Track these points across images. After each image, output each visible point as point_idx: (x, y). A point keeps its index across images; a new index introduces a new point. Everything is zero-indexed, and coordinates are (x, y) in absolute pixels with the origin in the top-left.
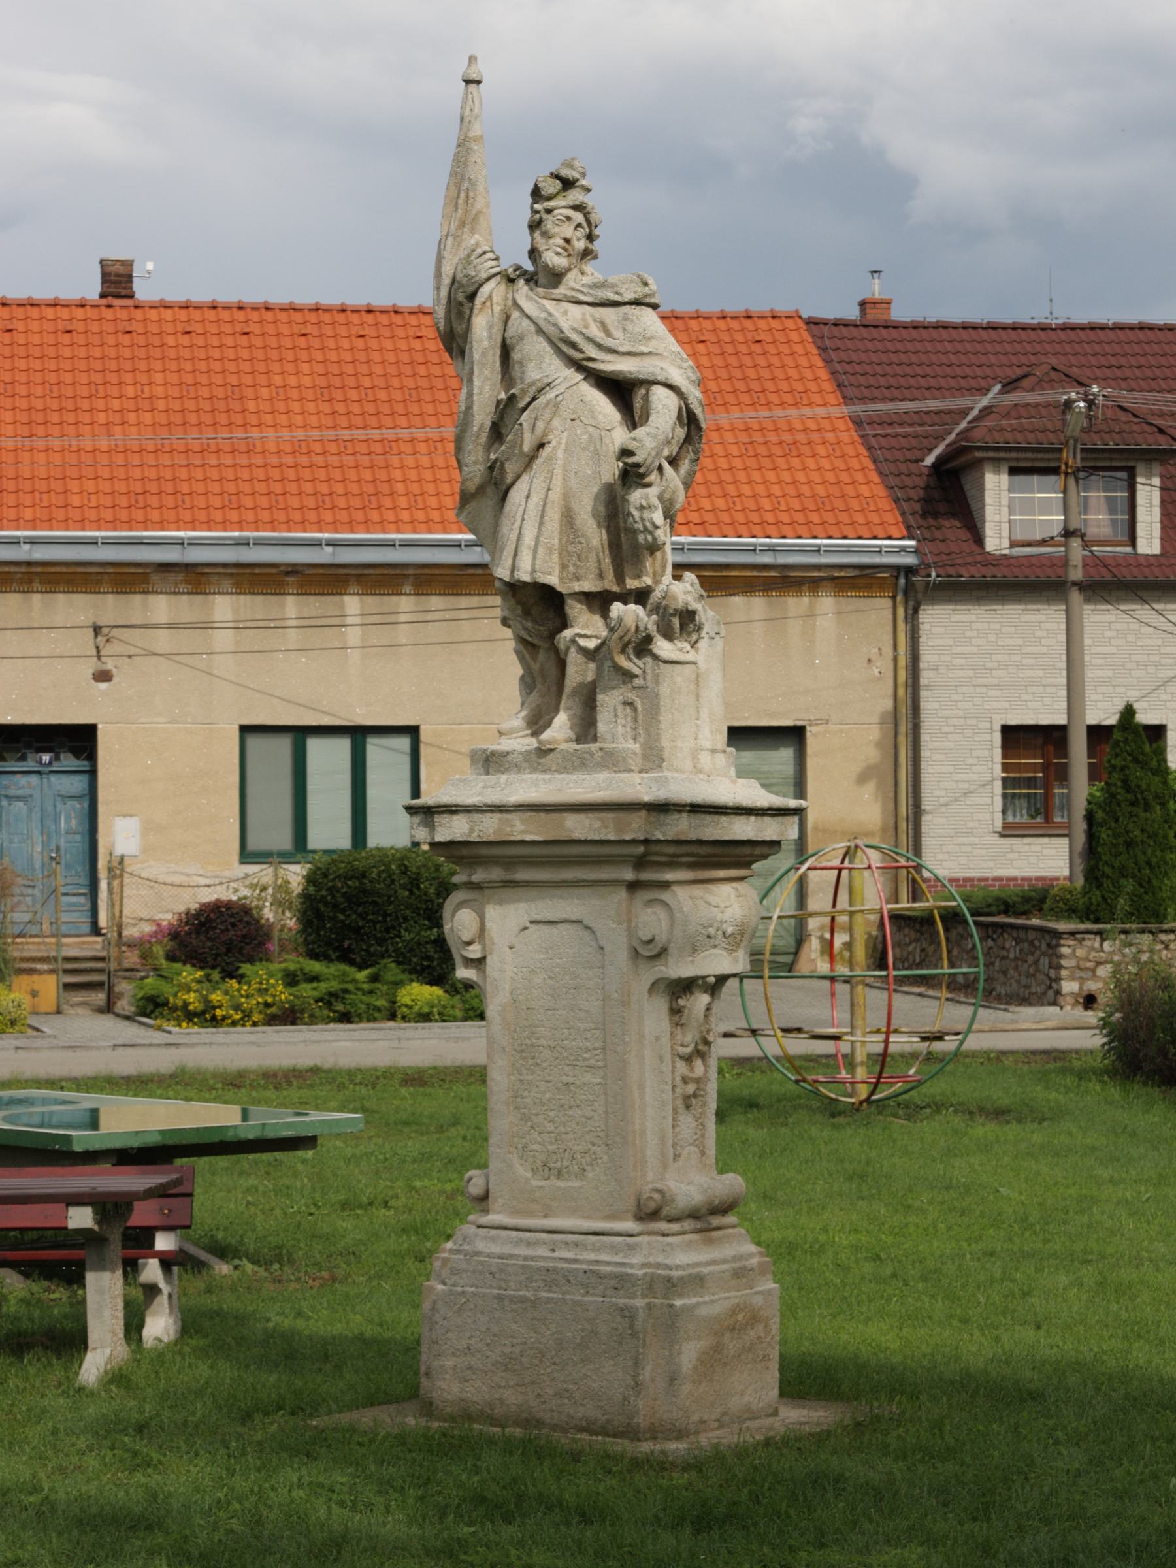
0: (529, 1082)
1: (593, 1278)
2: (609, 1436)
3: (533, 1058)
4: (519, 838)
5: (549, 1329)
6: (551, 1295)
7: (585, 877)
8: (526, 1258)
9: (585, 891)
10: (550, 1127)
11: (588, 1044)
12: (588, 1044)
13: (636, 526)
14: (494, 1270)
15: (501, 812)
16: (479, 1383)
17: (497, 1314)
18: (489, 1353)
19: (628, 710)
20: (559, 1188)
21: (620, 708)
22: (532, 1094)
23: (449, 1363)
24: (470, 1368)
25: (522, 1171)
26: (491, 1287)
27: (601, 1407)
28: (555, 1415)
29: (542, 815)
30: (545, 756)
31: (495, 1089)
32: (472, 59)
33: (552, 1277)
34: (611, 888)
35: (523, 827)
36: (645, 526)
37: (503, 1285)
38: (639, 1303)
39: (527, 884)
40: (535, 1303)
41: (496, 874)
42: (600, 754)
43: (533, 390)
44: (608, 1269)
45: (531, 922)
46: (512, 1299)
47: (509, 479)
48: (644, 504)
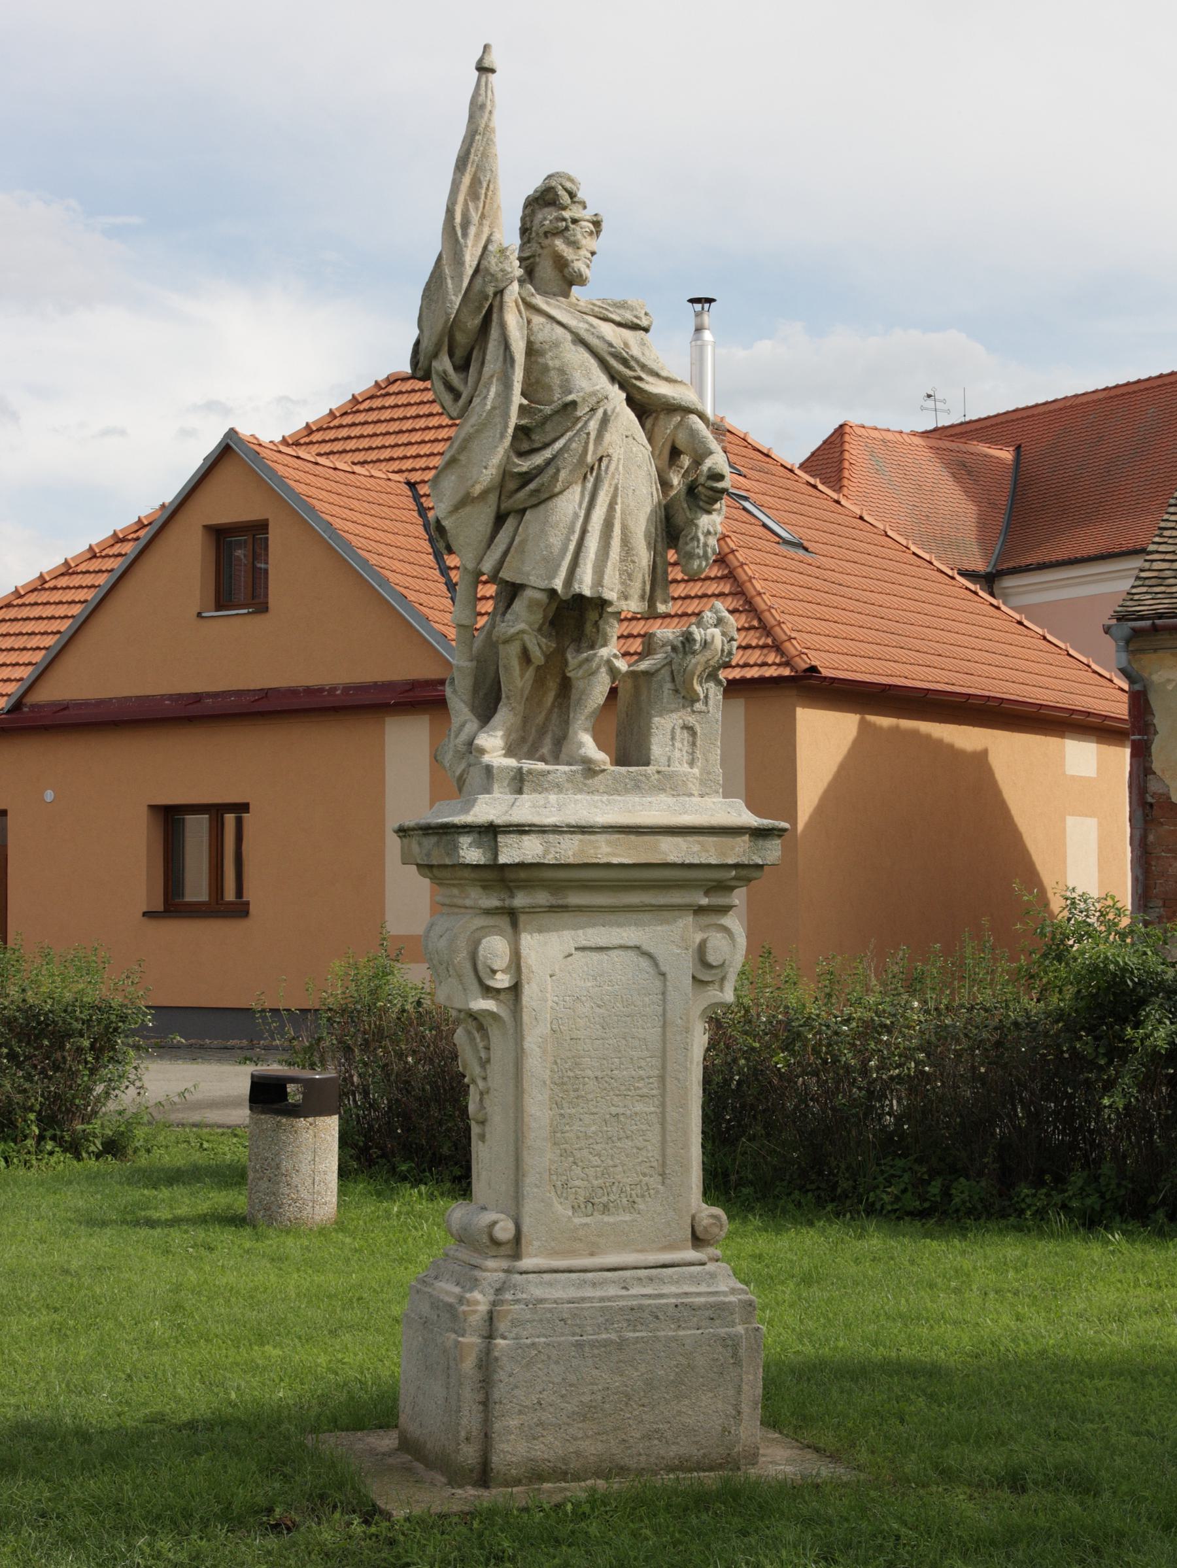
0: (570, 1116)
1: (683, 1311)
2: (704, 1471)
3: (576, 1090)
4: (604, 860)
5: (637, 1370)
6: (637, 1334)
7: (654, 901)
8: (602, 1299)
9: (646, 917)
10: (596, 1160)
11: (641, 1072)
12: (641, 1072)
13: (697, 551)
14: (565, 1316)
15: (583, 833)
16: (550, 1438)
17: (575, 1362)
18: (563, 1405)
19: (686, 734)
20: (608, 1223)
21: (678, 731)
22: (575, 1128)
23: (513, 1423)
24: (540, 1424)
25: (562, 1210)
26: (562, 1334)
27: (697, 1443)
28: (643, 1458)
29: (633, 837)
30: (592, 777)
31: (534, 1125)
32: (486, 48)
33: (636, 1315)
34: (677, 913)
35: (609, 850)
36: (705, 552)
37: (578, 1331)
38: (740, 1329)
39: (580, 909)
40: (621, 1345)
41: (542, 898)
42: (657, 776)
43: (593, 400)
44: (702, 1300)
45: (576, 949)
46: (593, 1345)
47: (557, 490)
48: (712, 530)
